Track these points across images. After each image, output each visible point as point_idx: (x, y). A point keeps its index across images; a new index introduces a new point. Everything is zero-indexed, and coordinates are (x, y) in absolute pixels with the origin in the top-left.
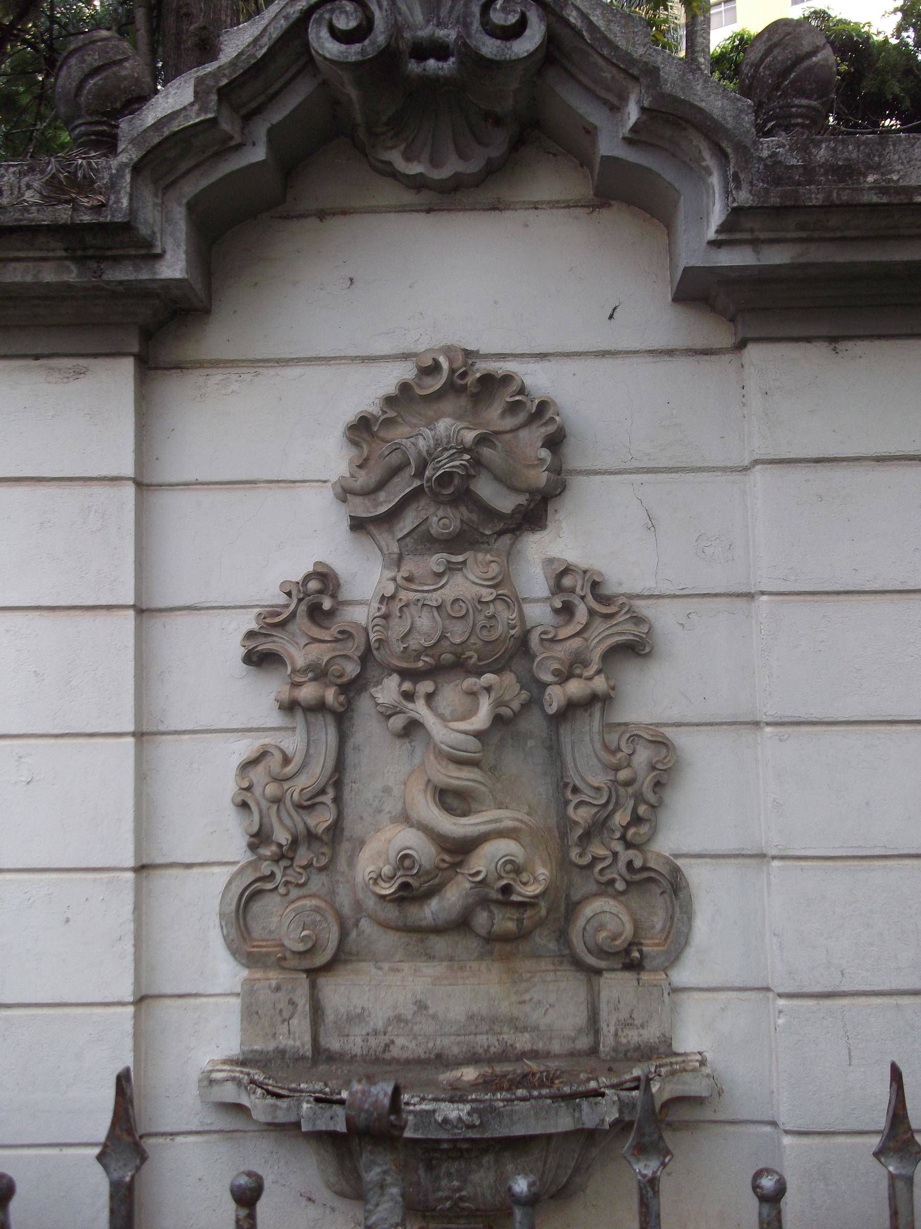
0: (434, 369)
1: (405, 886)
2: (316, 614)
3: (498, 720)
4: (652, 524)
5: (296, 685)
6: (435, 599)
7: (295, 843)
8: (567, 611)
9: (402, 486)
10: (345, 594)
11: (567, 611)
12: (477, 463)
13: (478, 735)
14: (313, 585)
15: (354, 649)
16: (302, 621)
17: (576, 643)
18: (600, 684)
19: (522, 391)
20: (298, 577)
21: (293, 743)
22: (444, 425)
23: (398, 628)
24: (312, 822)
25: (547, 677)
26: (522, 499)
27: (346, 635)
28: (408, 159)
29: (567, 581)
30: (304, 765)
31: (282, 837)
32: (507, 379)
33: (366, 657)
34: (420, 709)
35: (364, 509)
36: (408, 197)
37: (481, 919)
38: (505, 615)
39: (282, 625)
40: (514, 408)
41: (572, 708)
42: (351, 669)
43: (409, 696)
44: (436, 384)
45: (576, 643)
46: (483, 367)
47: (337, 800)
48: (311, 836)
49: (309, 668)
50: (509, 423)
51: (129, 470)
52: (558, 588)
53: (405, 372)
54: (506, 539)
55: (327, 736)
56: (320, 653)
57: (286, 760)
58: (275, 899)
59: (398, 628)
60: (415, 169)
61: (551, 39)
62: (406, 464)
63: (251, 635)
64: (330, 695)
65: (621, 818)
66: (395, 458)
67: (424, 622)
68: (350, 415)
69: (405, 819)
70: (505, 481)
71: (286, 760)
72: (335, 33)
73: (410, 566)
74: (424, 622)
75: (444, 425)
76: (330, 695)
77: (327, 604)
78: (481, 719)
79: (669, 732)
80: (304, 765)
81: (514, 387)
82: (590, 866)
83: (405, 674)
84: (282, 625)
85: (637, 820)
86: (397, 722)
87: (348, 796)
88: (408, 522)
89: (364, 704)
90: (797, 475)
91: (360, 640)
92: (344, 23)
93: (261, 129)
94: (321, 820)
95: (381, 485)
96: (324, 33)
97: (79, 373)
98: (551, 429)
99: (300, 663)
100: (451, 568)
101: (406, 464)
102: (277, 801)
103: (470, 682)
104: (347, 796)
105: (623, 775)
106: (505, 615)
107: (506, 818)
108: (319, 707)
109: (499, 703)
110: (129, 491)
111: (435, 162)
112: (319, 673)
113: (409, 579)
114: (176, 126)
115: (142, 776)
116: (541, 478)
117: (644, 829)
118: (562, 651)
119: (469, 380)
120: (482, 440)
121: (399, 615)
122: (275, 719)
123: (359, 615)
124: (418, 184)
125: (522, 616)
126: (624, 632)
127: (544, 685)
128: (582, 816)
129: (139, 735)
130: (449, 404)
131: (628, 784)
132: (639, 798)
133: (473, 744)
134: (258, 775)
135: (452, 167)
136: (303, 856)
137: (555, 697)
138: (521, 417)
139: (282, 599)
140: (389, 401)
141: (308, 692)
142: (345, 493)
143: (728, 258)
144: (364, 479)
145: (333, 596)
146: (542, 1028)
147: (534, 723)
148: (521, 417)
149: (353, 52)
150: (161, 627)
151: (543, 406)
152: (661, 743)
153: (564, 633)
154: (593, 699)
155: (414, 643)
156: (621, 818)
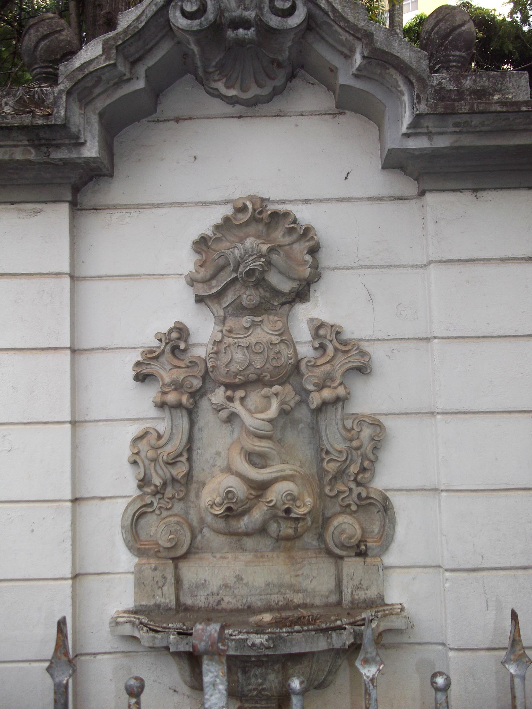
1: (229, 509)
4: (370, 298)
5: (164, 393)
6: (245, 342)
8: (322, 347)
9: (225, 278)
10: (192, 340)
11: (322, 347)
12: (269, 263)
13: (270, 421)
14: (174, 335)
15: (199, 371)
16: (168, 354)
17: (327, 367)
18: (341, 391)
20: (165, 330)
21: (162, 427)
22: (249, 242)
25: (310, 387)
26: (295, 284)
27: (193, 363)
28: (228, 87)
29: (322, 332)
30: (169, 440)
31: (157, 481)
32: (286, 214)
33: (205, 377)
34: (237, 406)
36: (229, 109)
37: (273, 527)
38: (286, 352)
39: (157, 358)
40: (291, 231)
42: (197, 383)
43: (230, 399)
44: (244, 217)
45: (327, 367)
46: (272, 208)
47: (189, 459)
48: (174, 480)
50: (287, 240)
51: (66, 269)
53: (228, 210)
55: (183, 422)
56: (179, 375)
57: (159, 437)
59: (224, 359)
60: (232, 93)
63: (138, 364)
64: (185, 399)
66: (221, 261)
67: (239, 356)
68: (195, 236)
69: (229, 470)
73: (231, 323)
74: (239, 356)
76: (185, 399)
78: (273, 411)
79: (382, 419)
80: (169, 440)
81: (291, 220)
82: (337, 496)
83: (228, 386)
84: (157, 358)
85: (363, 470)
86: (224, 414)
88: (229, 298)
89: (204, 404)
90: (454, 270)
91: (202, 367)
93: (141, 70)
94: (180, 471)
95: (213, 277)
96: (178, 14)
97: (37, 212)
98: (312, 243)
99: (167, 380)
102: (154, 460)
103: (266, 391)
104: (195, 457)
105: (355, 444)
106: (286, 352)
107: (288, 469)
108: (179, 406)
110: (66, 281)
111: (243, 90)
112: (178, 386)
113: (230, 331)
114: (92, 68)
115: (75, 447)
116: (306, 272)
118: (319, 372)
119: (265, 215)
120: (271, 250)
122: (153, 412)
123: (201, 352)
124: (232, 101)
126: (356, 360)
127: (309, 392)
128: (332, 467)
129: (74, 423)
130: (253, 229)
132: (364, 457)
133: (268, 427)
134: (143, 446)
135: (254, 91)
136: (169, 492)
137: (316, 399)
138: (295, 237)
139: (156, 343)
140: (217, 227)
141: (172, 398)
142: (192, 281)
143: (413, 144)
144: (203, 274)
145: (186, 341)
147: (303, 414)
148: (295, 237)
149: (195, 25)
152: (377, 425)
154: (338, 400)
155: (233, 368)
156: (354, 469)
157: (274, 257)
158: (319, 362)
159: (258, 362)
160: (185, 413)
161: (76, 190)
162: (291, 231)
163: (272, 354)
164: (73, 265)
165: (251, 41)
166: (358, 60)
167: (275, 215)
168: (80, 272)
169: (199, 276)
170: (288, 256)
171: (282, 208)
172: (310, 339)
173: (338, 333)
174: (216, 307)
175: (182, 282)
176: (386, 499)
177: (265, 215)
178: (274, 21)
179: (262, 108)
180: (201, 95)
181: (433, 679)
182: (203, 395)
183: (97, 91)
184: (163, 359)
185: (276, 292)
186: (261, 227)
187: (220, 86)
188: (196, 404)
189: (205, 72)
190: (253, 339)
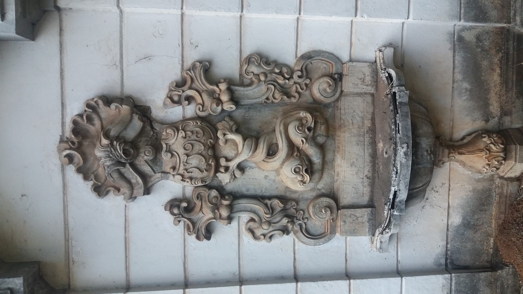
0: (70, 158)
2: (189, 210)
3: (238, 131)
5: (221, 217)
8: (189, 99)
12: (118, 138)
13: (244, 140)
14: (176, 211)
15: (205, 192)
18: (223, 86)
19: (81, 116)
20: (172, 218)
21: (245, 217)
22: (99, 153)
23: (196, 174)
25: (219, 108)
26: (136, 117)
29: (176, 98)
30: (254, 212)
31: (285, 221)
32: (75, 122)
34: (233, 164)
37: (321, 140)
39: (194, 224)
40: (90, 120)
41: (234, 100)
42: (214, 193)
43: (227, 169)
44: (78, 157)
45: (205, 96)
46: (68, 133)
47: (270, 198)
49: (213, 212)
50: (97, 122)
53: (71, 170)
54: (157, 126)
55: (243, 203)
57: (252, 220)
59: (196, 174)
63: (198, 238)
65: (281, 81)
66: (115, 175)
70: (127, 124)
71: (252, 220)
74: (194, 161)
75: (99, 153)
77: (185, 204)
78: (238, 138)
80: (254, 212)
81: (79, 119)
82: (299, 93)
83: (217, 171)
84: (194, 224)
86: (238, 173)
88: (147, 169)
94: (277, 204)
95: (128, 181)
98: (100, 102)
99: (211, 215)
100: (169, 150)
103: (221, 142)
104: (267, 194)
105: (262, 78)
108: (231, 207)
109: (231, 131)
112: (216, 207)
113: (174, 168)
116: (125, 109)
117: (285, 70)
118: (208, 101)
119: (75, 140)
120: (107, 136)
122: (234, 223)
126: (199, 73)
127: (223, 110)
131: (266, 75)
134: (258, 232)
136: (292, 211)
137: (229, 107)
138: (94, 116)
139: (182, 223)
140: (86, 178)
141: (224, 213)
142: (132, 197)
144: (125, 189)
145: (181, 201)
148: (94, 116)
151: (88, 106)
152: (249, 60)
153: (199, 100)
154: (229, 90)
155: (203, 166)
156: (281, 81)
157: (112, 133)
158: (199, 100)
159: (199, 147)
160: (236, 202)
162: (90, 120)
170: (112, 122)
171: (69, 126)
175: (134, 206)
177: (75, 140)
185: (142, 132)
186: (86, 143)
190: (181, 151)
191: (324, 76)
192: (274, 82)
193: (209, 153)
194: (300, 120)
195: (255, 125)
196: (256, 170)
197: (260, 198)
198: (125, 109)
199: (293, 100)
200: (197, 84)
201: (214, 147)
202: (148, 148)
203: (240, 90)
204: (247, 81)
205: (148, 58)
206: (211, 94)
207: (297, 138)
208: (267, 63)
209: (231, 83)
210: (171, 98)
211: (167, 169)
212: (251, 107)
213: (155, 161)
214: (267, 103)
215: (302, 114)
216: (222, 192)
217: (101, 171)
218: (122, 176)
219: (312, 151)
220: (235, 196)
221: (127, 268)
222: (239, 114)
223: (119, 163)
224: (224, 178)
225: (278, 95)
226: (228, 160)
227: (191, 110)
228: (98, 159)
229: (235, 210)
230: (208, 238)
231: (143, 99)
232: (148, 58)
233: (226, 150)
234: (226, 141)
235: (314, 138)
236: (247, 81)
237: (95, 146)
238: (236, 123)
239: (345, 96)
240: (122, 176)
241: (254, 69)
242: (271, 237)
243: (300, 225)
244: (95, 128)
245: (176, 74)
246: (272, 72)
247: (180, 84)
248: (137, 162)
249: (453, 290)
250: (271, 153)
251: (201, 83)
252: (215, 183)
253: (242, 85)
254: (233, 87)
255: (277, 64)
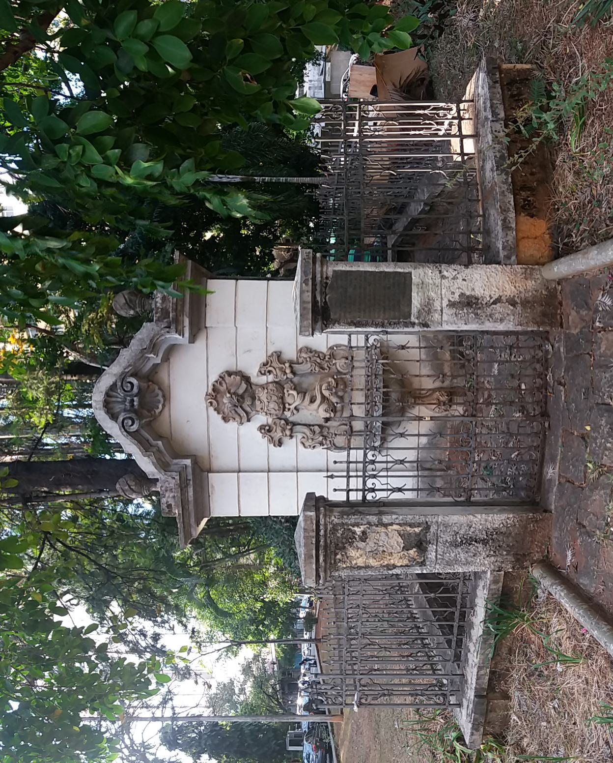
0: (211, 403)
1: (332, 411)
2: (269, 431)
3: (295, 389)
5: (286, 435)
6: (266, 403)
7: (323, 436)
8: (270, 372)
9: (240, 410)
10: (265, 423)
11: (270, 372)
12: (234, 393)
13: (298, 394)
14: (263, 431)
15: (278, 421)
16: (271, 434)
17: (277, 370)
18: (287, 365)
19: (216, 382)
20: (261, 435)
21: (300, 436)
23: (273, 412)
24: (317, 432)
25: (285, 377)
26: (243, 382)
27: (275, 423)
28: (158, 408)
29: (263, 372)
30: (304, 433)
31: (321, 438)
32: (214, 385)
34: (292, 407)
35: (245, 419)
36: (166, 409)
37: (340, 394)
39: (272, 438)
40: (221, 384)
41: (293, 372)
42: (283, 422)
43: (289, 409)
44: (214, 402)
45: (277, 370)
46: (210, 391)
47: (313, 426)
48: (321, 432)
49: (282, 432)
50: (224, 385)
51: (236, 474)
52: (264, 374)
53: (211, 409)
54: (253, 387)
55: (298, 428)
56: (279, 430)
57: (304, 437)
58: (335, 440)
59: (273, 412)
60: (160, 406)
61: (132, 375)
62: (235, 410)
63: (274, 445)
64: (289, 427)
65: (318, 360)
66: (233, 412)
68: (223, 421)
71: (304, 437)
72: (132, 425)
74: (272, 405)
75: (225, 401)
76: (289, 427)
77: (267, 428)
78: (295, 393)
79: (299, 348)
80: (304, 433)
81: (216, 384)
82: (329, 368)
83: (284, 410)
84: (272, 438)
85: (319, 357)
86: (295, 412)
87: (312, 423)
88: (248, 409)
89: (291, 419)
91: (275, 420)
92: (130, 422)
94: (317, 429)
95: (240, 415)
96: (132, 427)
97: (213, 486)
98: (226, 375)
99: (281, 434)
100: (259, 400)
101: (235, 410)
102: (312, 439)
103: (286, 395)
104: (312, 423)
105: (308, 359)
107: (318, 387)
108: (291, 430)
109: (291, 389)
110: (240, 474)
111: (159, 402)
112: (283, 430)
113: (262, 409)
114: (155, 461)
116: (238, 378)
117: (321, 355)
118: (279, 373)
119: (214, 394)
120: (229, 393)
121: (170, 701)
122: (294, 439)
123: (270, 421)
124: (164, 406)
125: (271, 383)
127: (287, 378)
129: (297, 471)
130: (219, 399)
131: (310, 358)
132: (314, 356)
133: (300, 395)
134: (307, 444)
135: (160, 398)
136: (325, 434)
137: (290, 376)
138: (223, 382)
139: (266, 438)
140: (218, 413)
141: (288, 433)
142: (242, 423)
143: (187, 334)
144: (238, 419)
145: (266, 426)
146: (530, 299)
147: (296, 380)
148: (223, 382)
149: (137, 423)
150: (271, 468)
151: (220, 377)
152: (301, 351)
153: (275, 373)
154: (290, 366)
155: (277, 408)
156: (318, 360)
157: (232, 391)
158: (275, 373)
160: (294, 427)
161: (202, 471)
162: (221, 384)
163: (272, 392)
164: (234, 472)
165: (139, 399)
166: (152, 355)
167: (214, 390)
168: (237, 469)
169: (239, 421)
170: (231, 385)
171: (211, 387)
172: (265, 377)
173: (264, 365)
174: (252, 414)
175: (241, 427)
176: (330, 348)
177: (214, 394)
178: (135, 390)
179: (167, 396)
180: (161, 418)
181: (328, 404)
182: (287, 419)
183: (163, 460)
184: (273, 436)
186: (218, 396)
187: (157, 411)
188: (291, 422)
189: (151, 417)
190: (265, 400)
191: (343, 358)
192: (315, 362)
193: (324, 392)
194: (329, 383)
195: (305, 386)
196: (305, 410)
197: (308, 426)
198: (238, 378)
199: (326, 371)
200: (273, 364)
201: (282, 398)
202: (249, 398)
203: (296, 366)
204: (300, 361)
205: (249, 351)
206: (281, 369)
207: (326, 393)
208: (311, 352)
209: (291, 363)
210: (261, 372)
211: (258, 409)
212: (302, 375)
213: (253, 405)
214: (311, 373)
215: (330, 379)
216: (287, 422)
217: (226, 410)
218: (236, 412)
219: (334, 400)
220: (294, 424)
221: (239, 461)
222: (296, 380)
223: (235, 406)
224: (288, 414)
225: (317, 369)
226: (289, 405)
227: (271, 378)
228: (224, 404)
229: (294, 431)
230: (280, 446)
231: (247, 372)
232: (249, 351)
233: (288, 400)
234: (289, 395)
235: (336, 393)
236: (300, 361)
237: (223, 397)
238: (294, 384)
239: (356, 368)
240: (236, 412)
241: (304, 355)
242: (314, 447)
243: (330, 441)
244: (223, 388)
245: (264, 359)
246: (313, 356)
247: (264, 365)
248: (243, 405)
249: (84, 361)
250: (312, 401)
251: (276, 364)
252: (283, 417)
253: (298, 363)
254: (293, 365)
255: (316, 351)
